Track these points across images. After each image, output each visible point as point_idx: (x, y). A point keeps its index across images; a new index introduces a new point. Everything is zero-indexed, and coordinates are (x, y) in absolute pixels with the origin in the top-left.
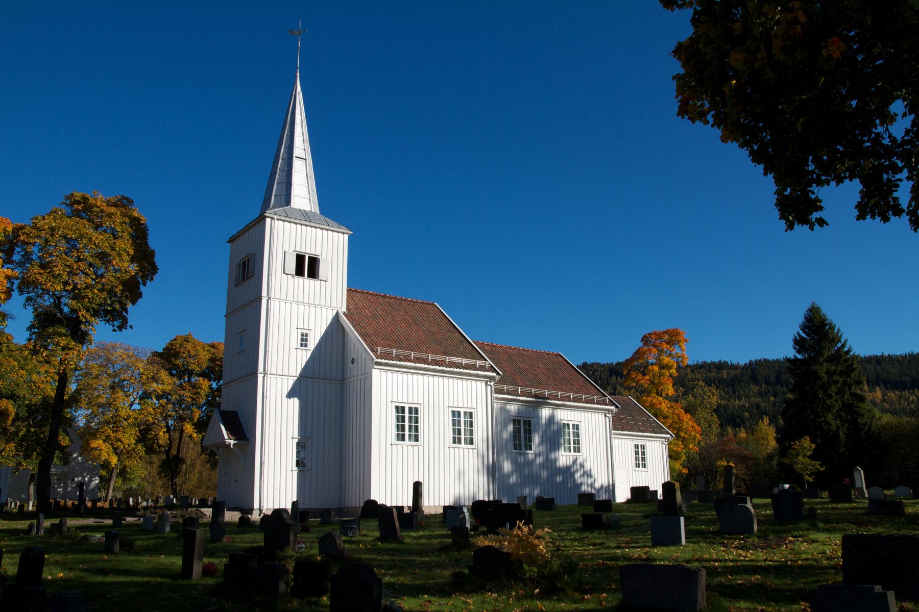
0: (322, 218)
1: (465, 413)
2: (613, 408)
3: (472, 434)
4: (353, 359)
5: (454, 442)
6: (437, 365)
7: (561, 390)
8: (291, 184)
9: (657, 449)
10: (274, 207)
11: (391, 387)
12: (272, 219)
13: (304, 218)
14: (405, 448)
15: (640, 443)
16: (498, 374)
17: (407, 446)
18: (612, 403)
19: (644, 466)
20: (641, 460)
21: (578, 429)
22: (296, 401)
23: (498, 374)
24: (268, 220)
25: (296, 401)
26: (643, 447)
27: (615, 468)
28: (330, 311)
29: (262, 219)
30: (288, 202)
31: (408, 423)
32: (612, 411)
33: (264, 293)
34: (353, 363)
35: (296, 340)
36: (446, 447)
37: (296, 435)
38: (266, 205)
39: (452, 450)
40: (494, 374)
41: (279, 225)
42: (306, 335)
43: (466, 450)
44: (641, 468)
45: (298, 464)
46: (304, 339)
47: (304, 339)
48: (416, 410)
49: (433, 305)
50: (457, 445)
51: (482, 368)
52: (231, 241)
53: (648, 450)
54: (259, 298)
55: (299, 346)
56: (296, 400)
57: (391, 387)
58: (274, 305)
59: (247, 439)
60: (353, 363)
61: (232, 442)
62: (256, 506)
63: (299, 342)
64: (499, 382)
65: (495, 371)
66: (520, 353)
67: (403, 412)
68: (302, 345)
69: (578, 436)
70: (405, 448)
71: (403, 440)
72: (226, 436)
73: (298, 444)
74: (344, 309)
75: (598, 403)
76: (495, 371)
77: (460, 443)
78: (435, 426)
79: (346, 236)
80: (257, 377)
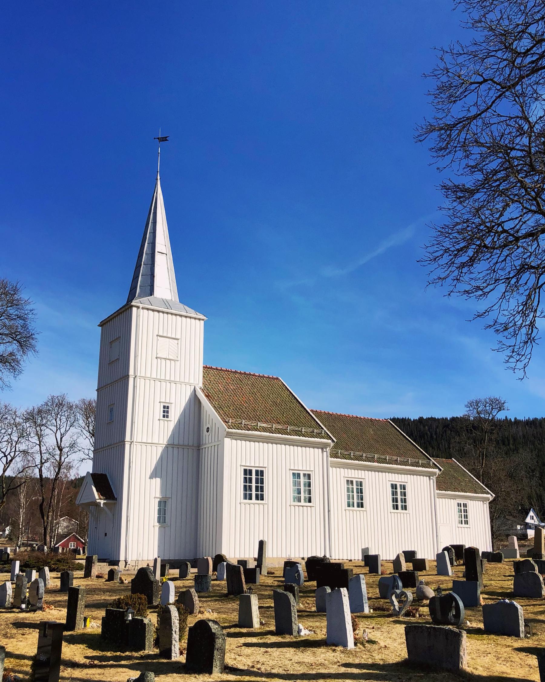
0: (181, 305)
1: (304, 475)
2: (437, 470)
3: (362, 499)
4: (208, 428)
5: (245, 498)
6: (279, 433)
7: (389, 454)
8: (154, 277)
9: (479, 510)
10: (140, 296)
11: (238, 454)
12: (138, 307)
13: (164, 309)
14: (355, 512)
15: (462, 502)
16: (333, 441)
17: (254, 504)
18: (436, 466)
19: (466, 522)
20: (464, 519)
21: (404, 489)
22: (157, 481)
23: (333, 441)
24: (134, 309)
25: (157, 481)
26: (465, 505)
27: (439, 525)
28: (188, 387)
29: (127, 308)
30: (151, 293)
31: (254, 484)
32: (435, 474)
33: (131, 372)
34: (208, 431)
35: (159, 411)
36: (288, 504)
37: (158, 495)
38: (132, 296)
39: (243, 505)
40: (330, 441)
41: (144, 313)
42: (168, 407)
43: (257, 506)
44: (463, 525)
45: (159, 521)
46: (166, 410)
47: (166, 410)
48: (262, 472)
49: (277, 379)
50: (248, 501)
51: (319, 436)
52: (102, 324)
53: (469, 508)
54: (127, 376)
55: (162, 418)
56: (158, 480)
57: (238, 454)
58: (140, 383)
59: (116, 499)
60: (208, 431)
61: (102, 502)
62: (122, 558)
63: (162, 414)
64: (334, 447)
65: (330, 438)
66: (355, 420)
67: (396, 488)
68: (164, 416)
69: (405, 495)
70: (361, 512)
71: (397, 509)
72: (97, 497)
73: (160, 502)
74: (201, 385)
75: (423, 466)
76: (330, 438)
77: (251, 498)
78: (279, 486)
79: (202, 322)
80: (124, 445)
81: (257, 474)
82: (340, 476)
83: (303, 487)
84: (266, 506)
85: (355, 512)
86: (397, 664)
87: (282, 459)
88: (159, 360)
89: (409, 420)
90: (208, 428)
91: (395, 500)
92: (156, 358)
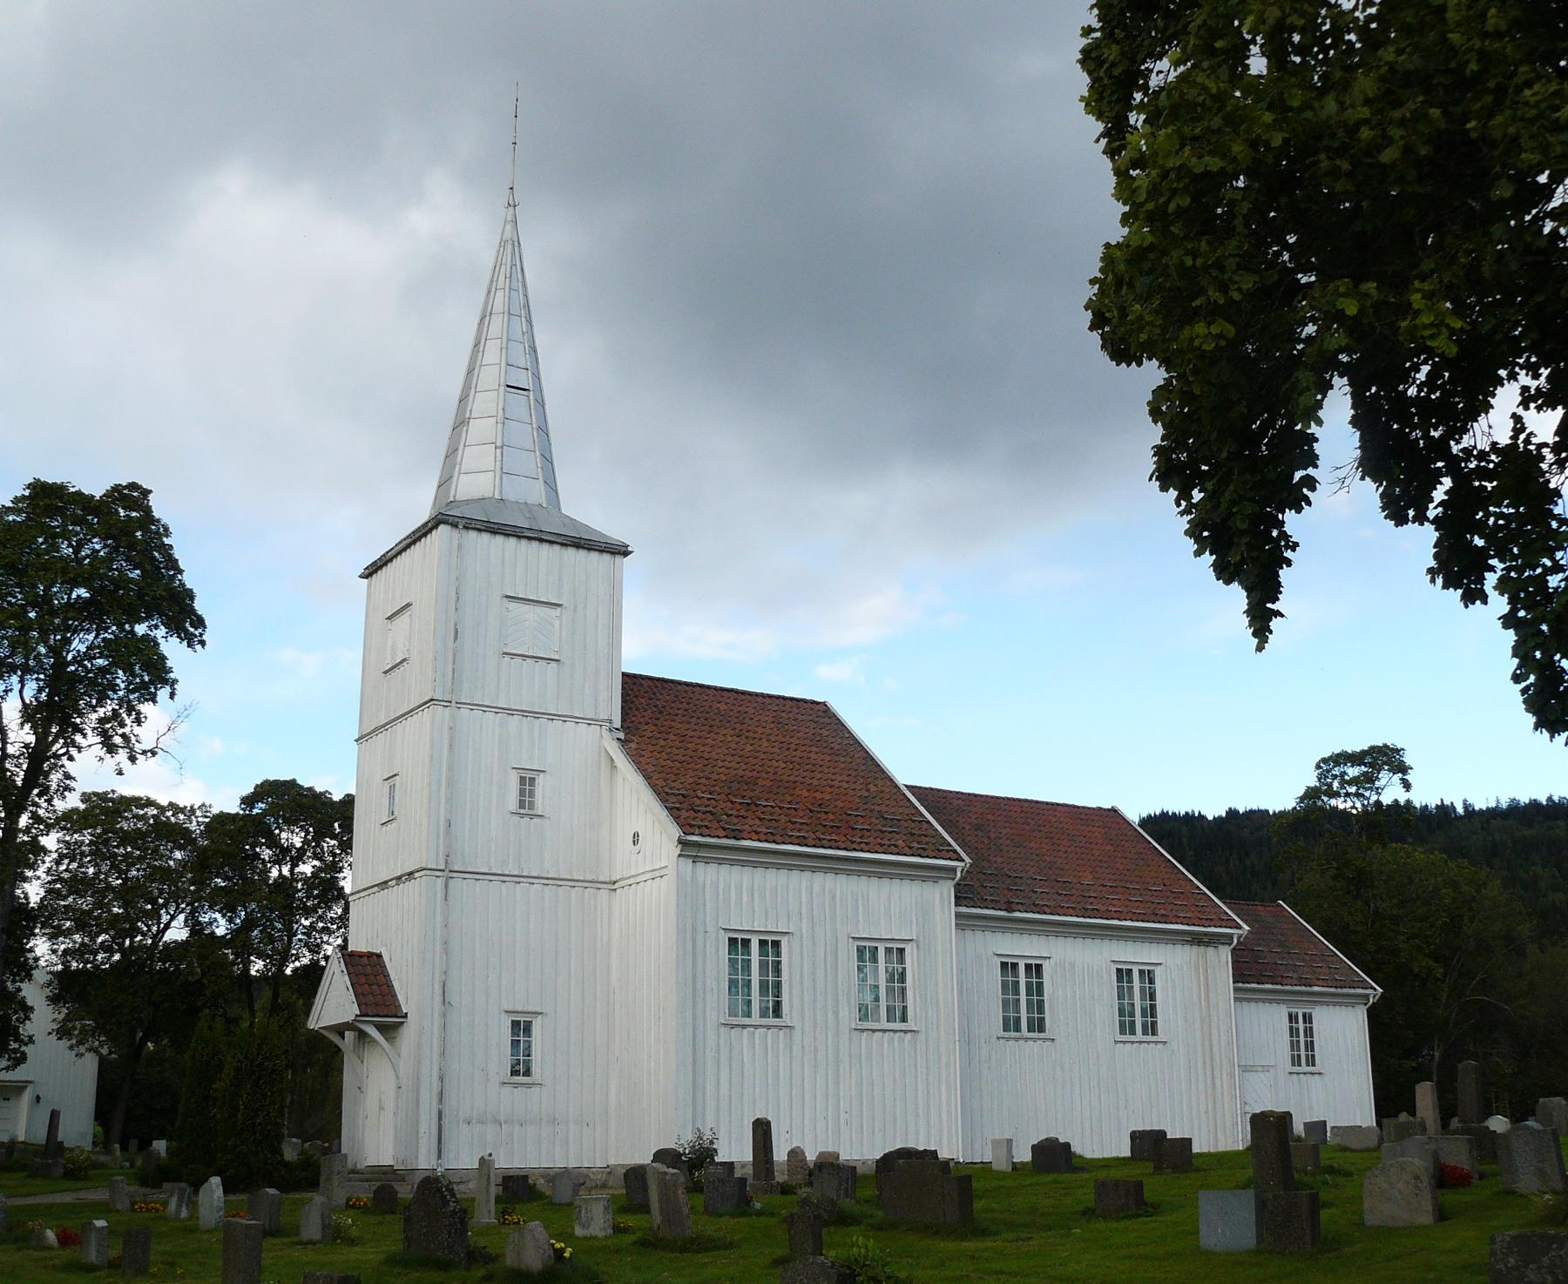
78: (816, 978)
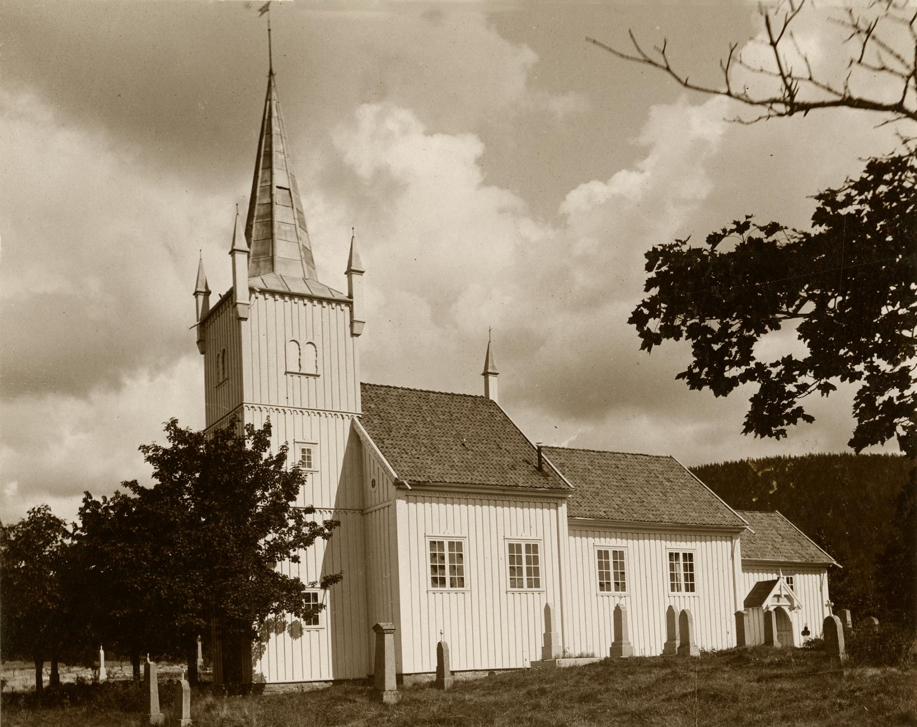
4: (374, 481)
11: (417, 524)
14: (611, 598)
31: (447, 567)
34: (373, 486)
57: (417, 524)
60: (373, 486)
78: (486, 563)
81: (443, 581)
82: (583, 552)
83: (524, 565)
84: (468, 595)
85: (611, 598)
86: (722, 653)
87: (486, 529)
88: (289, 375)
89: (717, 465)
90: (374, 481)
91: (689, 567)
92: (286, 373)
